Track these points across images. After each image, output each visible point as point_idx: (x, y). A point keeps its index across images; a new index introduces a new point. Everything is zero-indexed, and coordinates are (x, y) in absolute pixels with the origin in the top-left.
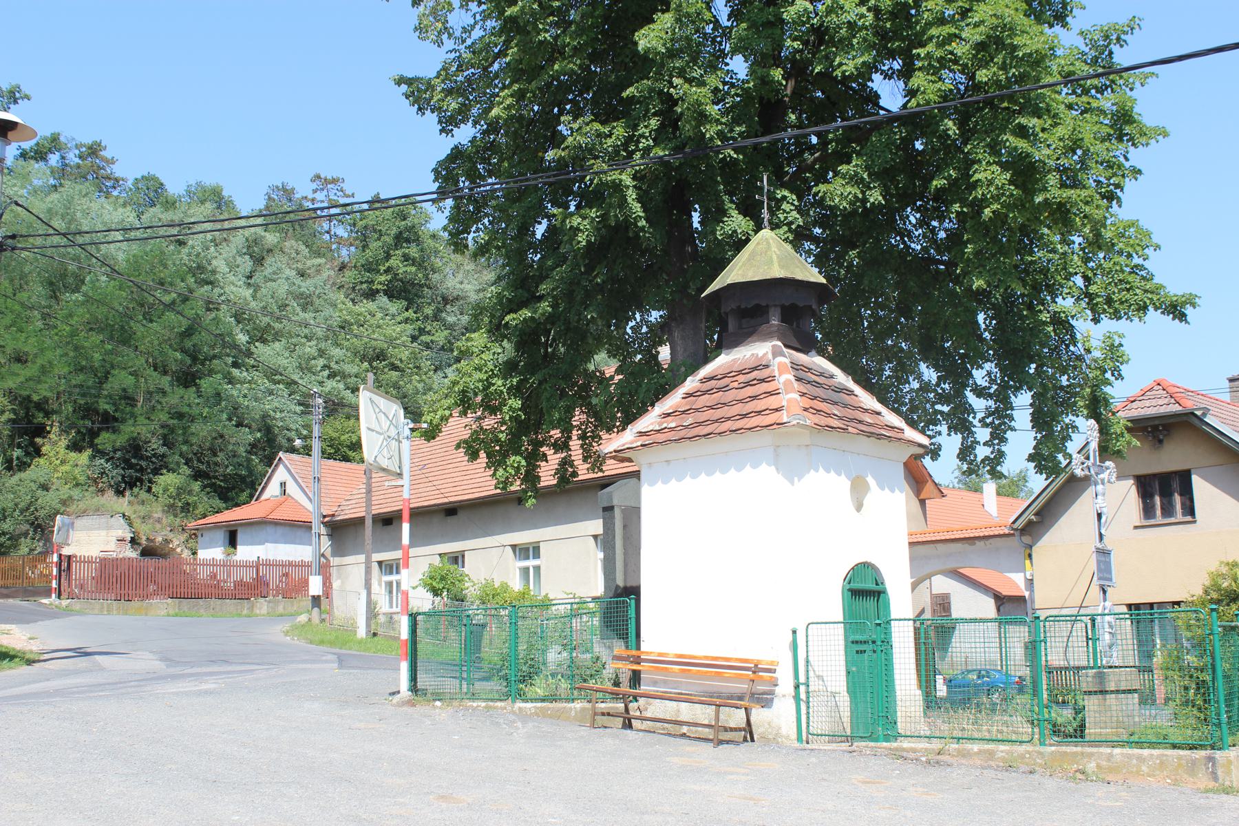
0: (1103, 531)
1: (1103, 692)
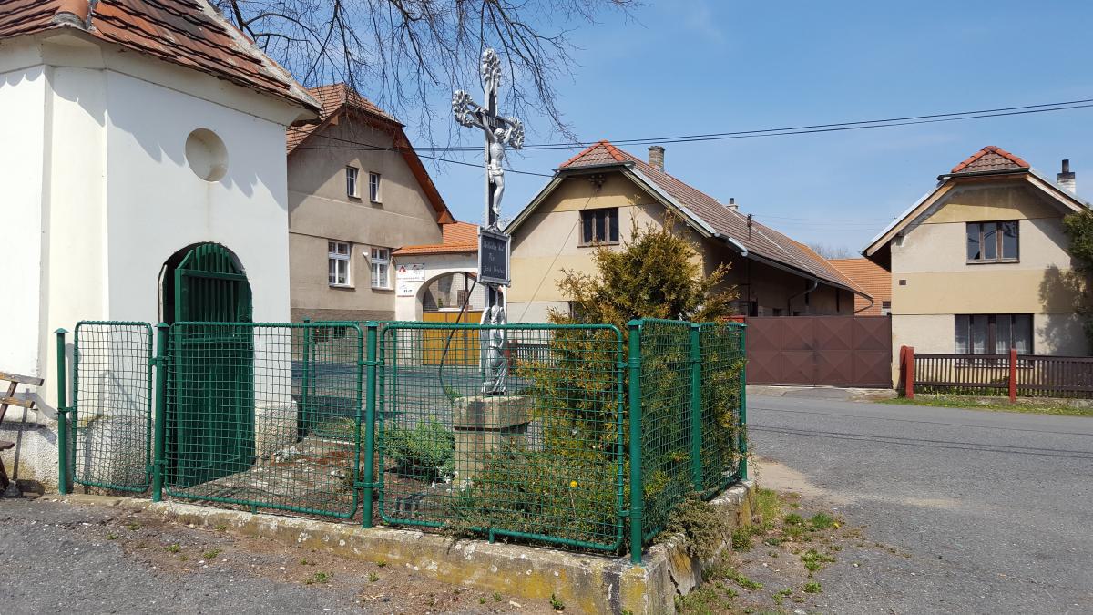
0: (495, 209)
1: (480, 429)
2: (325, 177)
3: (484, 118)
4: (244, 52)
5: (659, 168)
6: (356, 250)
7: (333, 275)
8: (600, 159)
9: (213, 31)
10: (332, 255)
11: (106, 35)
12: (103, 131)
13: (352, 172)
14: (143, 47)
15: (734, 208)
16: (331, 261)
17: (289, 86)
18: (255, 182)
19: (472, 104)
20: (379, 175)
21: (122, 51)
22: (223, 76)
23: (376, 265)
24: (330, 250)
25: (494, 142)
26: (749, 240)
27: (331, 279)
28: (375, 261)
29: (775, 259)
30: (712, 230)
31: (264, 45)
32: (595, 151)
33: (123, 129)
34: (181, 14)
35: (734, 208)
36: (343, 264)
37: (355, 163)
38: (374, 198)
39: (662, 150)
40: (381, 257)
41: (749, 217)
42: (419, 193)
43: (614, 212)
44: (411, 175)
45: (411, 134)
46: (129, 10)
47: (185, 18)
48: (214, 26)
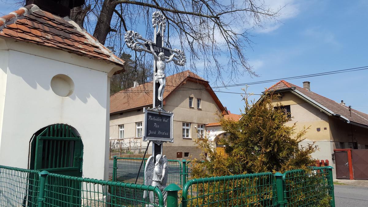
2: (182, 100)
3: (151, 47)
4: (90, 43)
5: (308, 90)
6: (192, 125)
7: (184, 134)
8: (282, 87)
9: (78, 36)
10: (184, 127)
11: (5, 34)
12: (6, 76)
13: (191, 99)
14: (25, 39)
15: (343, 104)
16: (184, 129)
17: (110, 56)
18: (89, 97)
19: (140, 39)
20: (200, 99)
21: (17, 41)
22: (70, 51)
23: (185, 129)
24: (183, 126)
25: (158, 60)
26: (351, 116)
27: (183, 136)
28: (199, 129)
29: (364, 124)
30: (332, 113)
31: (144, 54)
32: (279, 84)
33: (16, 75)
34: (62, 30)
35: (343, 104)
36: (188, 130)
37: (192, 96)
38: (199, 107)
39: (309, 83)
40: (201, 127)
41: (350, 107)
42: (215, 104)
43: (288, 107)
44: (212, 99)
45: (211, 85)
46: (30, 27)
47: (64, 31)
48: (38, 22)
